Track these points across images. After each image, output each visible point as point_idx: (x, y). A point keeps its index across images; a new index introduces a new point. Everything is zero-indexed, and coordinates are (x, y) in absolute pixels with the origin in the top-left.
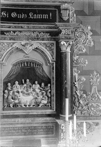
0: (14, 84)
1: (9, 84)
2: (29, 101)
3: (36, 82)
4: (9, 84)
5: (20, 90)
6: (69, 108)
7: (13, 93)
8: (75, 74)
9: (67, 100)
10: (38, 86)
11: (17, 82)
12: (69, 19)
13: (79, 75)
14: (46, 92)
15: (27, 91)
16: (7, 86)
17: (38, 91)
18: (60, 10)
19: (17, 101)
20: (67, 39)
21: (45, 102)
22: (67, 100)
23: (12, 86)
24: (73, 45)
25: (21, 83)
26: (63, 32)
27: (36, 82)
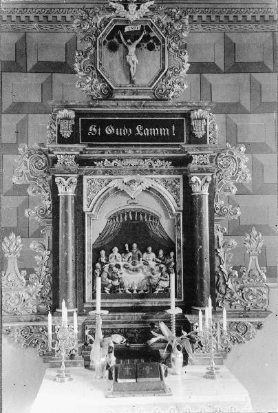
3: (150, 249)
4: (103, 252)
5: (121, 264)
7: (110, 267)
10: (153, 255)
11: (116, 249)
14: (168, 265)
17: (152, 264)
19: (116, 283)
23: (107, 256)
25: (123, 251)
27: (150, 249)
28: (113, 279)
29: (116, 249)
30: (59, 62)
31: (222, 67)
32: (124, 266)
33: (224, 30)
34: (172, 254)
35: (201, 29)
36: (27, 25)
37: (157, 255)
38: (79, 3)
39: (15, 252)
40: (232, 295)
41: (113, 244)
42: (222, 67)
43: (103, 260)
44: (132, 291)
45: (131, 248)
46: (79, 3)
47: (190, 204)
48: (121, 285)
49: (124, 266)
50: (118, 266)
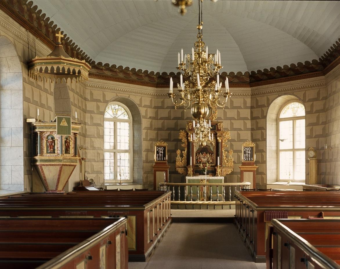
0: (200, 154)
1: (198, 154)
2: (205, 160)
3: (208, 153)
4: (198, 154)
5: (202, 156)
6: (92, 237)
7: (199, 157)
8: (223, 150)
9: (9, 217)
10: (209, 155)
11: (201, 153)
12: (221, 129)
13: (225, 151)
14: (212, 157)
15: (204, 157)
16: (197, 155)
17: (209, 157)
18: (217, 125)
19: (201, 160)
20: (220, 137)
21: (211, 161)
22: (9, 217)
23: (199, 155)
24: (269, 219)
25: (202, 154)
26: (218, 134)
27: (208, 153)
28: (200, 159)
29: (201, 153)
30: (144, 248)
31: (230, 108)
32: (202, 157)
33: (116, 92)
34: (213, 155)
35: (239, 97)
36: (178, 97)
37: (210, 155)
38: (199, 4)
39: (179, 153)
40: (226, 163)
41: (200, 152)
42: (230, 108)
43: (198, 155)
44: (204, 162)
45: (204, 153)
46: (199, 4)
47: (217, 143)
48: (202, 161)
49: (202, 157)
50: (201, 157)
